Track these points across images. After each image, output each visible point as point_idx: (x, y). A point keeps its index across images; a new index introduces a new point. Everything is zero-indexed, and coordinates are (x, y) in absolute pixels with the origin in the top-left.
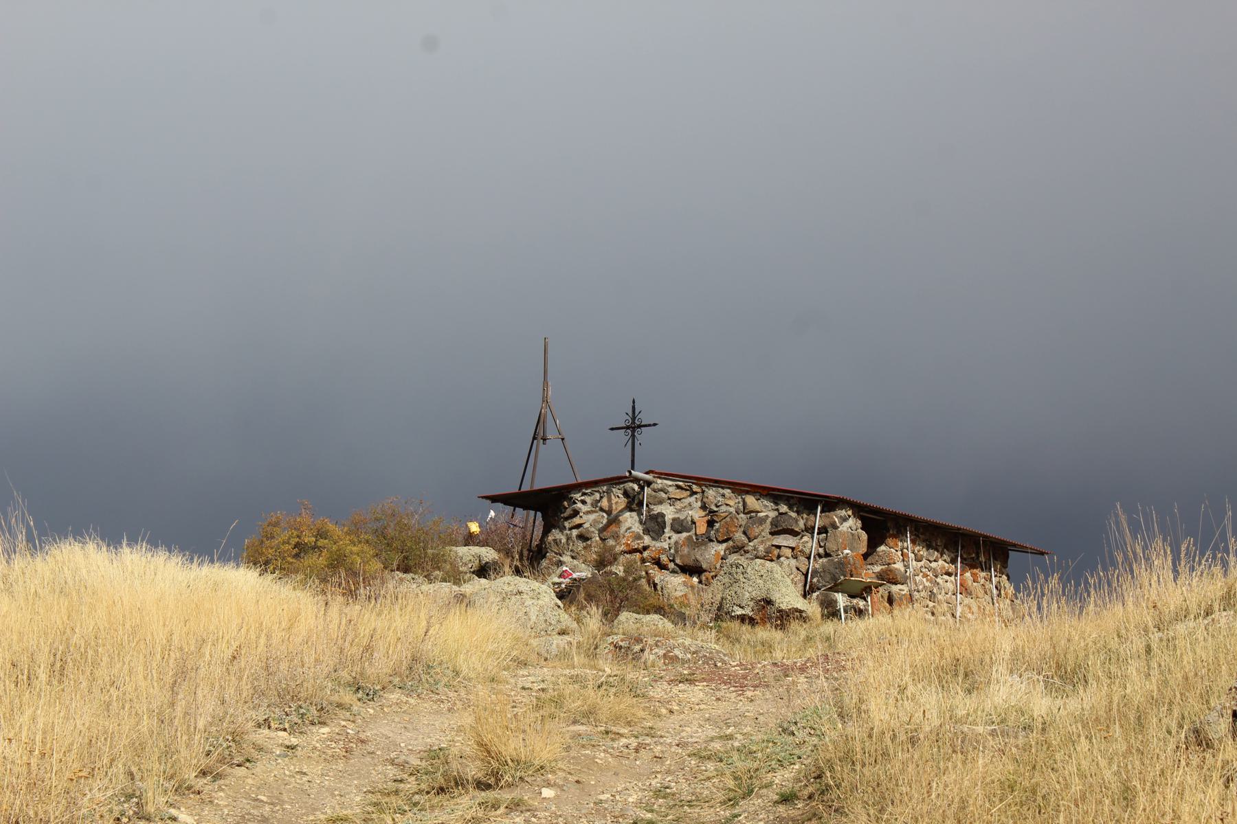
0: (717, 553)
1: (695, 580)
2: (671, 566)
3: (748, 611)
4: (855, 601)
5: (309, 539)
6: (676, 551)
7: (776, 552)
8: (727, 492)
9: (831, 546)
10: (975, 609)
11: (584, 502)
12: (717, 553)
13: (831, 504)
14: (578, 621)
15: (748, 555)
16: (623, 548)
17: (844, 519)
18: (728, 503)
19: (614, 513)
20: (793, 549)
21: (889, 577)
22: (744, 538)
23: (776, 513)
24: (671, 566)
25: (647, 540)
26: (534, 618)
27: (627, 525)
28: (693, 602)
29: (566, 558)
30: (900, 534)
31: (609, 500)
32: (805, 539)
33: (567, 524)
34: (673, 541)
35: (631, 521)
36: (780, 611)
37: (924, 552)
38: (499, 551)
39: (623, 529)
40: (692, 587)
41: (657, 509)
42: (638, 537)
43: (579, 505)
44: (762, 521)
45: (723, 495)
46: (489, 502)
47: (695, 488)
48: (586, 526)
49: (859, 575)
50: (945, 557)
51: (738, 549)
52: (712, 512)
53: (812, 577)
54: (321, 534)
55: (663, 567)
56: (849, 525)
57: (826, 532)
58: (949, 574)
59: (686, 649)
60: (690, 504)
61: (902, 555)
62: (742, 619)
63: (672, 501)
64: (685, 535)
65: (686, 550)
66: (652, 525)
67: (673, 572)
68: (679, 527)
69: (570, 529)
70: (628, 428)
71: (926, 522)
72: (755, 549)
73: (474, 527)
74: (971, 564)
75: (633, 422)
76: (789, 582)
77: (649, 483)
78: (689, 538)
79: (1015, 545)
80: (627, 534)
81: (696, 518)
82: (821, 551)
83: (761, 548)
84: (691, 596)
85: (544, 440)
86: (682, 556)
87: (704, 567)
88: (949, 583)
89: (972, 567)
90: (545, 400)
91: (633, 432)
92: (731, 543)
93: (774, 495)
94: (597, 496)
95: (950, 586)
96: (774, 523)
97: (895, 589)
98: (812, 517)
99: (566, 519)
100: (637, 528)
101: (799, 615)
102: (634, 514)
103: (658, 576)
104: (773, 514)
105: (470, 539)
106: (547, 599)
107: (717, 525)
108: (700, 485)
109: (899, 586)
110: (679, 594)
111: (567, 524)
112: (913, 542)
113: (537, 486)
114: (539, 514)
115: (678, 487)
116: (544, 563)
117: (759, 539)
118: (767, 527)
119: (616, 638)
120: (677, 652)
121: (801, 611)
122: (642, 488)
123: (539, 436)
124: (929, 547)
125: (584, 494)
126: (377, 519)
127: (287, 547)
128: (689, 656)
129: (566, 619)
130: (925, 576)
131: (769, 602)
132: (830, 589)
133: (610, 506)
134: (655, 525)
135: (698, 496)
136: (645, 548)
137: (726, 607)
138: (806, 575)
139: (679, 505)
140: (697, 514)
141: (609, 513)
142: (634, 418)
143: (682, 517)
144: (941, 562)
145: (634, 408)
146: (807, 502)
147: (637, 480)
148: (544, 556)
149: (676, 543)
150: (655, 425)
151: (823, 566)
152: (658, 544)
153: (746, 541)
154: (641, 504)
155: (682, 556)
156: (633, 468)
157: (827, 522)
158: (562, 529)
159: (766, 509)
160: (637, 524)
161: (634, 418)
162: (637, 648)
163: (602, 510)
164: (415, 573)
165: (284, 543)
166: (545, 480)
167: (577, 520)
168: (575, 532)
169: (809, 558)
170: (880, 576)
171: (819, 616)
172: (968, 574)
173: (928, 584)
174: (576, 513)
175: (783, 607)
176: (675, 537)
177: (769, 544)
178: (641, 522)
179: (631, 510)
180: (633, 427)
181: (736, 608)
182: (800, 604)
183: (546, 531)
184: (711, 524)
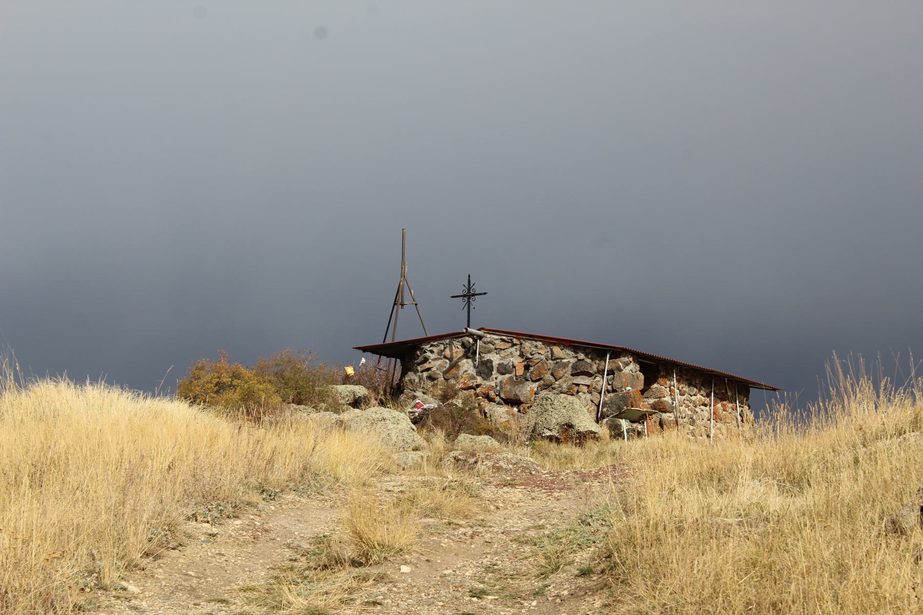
0: (532, 390)
1: (515, 409)
2: (497, 399)
3: (554, 433)
4: (635, 425)
5: (226, 379)
6: (501, 388)
7: (576, 388)
8: (539, 344)
9: (617, 384)
10: (724, 431)
11: (432, 352)
12: (532, 390)
13: (617, 353)
14: (428, 440)
15: (555, 391)
16: (461, 386)
17: (627, 364)
18: (540, 352)
19: (455, 359)
20: (588, 386)
21: (660, 408)
22: (551, 378)
23: (576, 360)
24: (497, 399)
25: (479, 380)
26: (394, 438)
27: (465, 368)
28: (514, 426)
29: (419, 394)
30: (668, 375)
31: (451, 350)
32: (598, 379)
33: (419, 368)
34: (498, 380)
35: (467, 366)
36: (579, 433)
37: (686, 389)
38: (368, 388)
39: (461, 372)
40: (513, 415)
41: (487, 357)
42: (473, 378)
43: (428, 354)
44: (565, 365)
45: (536, 347)
46: (361, 351)
47: (515, 341)
48: (433, 369)
49: (638, 406)
50: (702, 392)
51: (547, 386)
52: (528, 359)
53: (603, 407)
54: (235, 376)
55: (491, 400)
56: (630, 368)
57: (613, 374)
58: (705, 405)
59: (509, 461)
60: (511, 353)
61: (670, 391)
62: (551, 438)
63: (498, 350)
64: (508, 376)
65: (508, 387)
66: (483, 368)
67: (499, 403)
68: (503, 369)
69: (422, 372)
70: (464, 296)
71: (688, 366)
72: (560, 386)
73: (350, 371)
74: (721, 397)
75: (469, 292)
76: (586, 411)
77: (481, 338)
78: (511, 378)
79: (754, 383)
80: (465, 376)
81: (516, 363)
82: (609, 387)
83: (565, 386)
84: (512, 422)
85: (402, 305)
86: (505, 392)
87: (522, 399)
88: (705, 412)
89: (722, 399)
90: (403, 275)
91: (469, 299)
92: (542, 382)
93: (575, 346)
94: (442, 347)
95: (706, 414)
96: (574, 367)
97: (665, 416)
98: (603, 363)
99: (419, 364)
100: (472, 371)
101: (593, 435)
102: (470, 361)
103: (488, 407)
104: (573, 361)
105: (347, 380)
106: (404, 424)
107: (532, 369)
108: (519, 339)
109: (668, 414)
110: (503, 420)
111: (419, 368)
112: (678, 381)
113: (396, 340)
114: (398, 361)
115: (503, 340)
116: (402, 397)
117: (563, 379)
118: (569, 370)
119: (456, 453)
120: (501, 463)
121: (592, 432)
122: (475, 341)
123: (398, 302)
124: (690, 385)
125: (432, 346)
126: (277, 365)
127: (210, 385)
128: (511, 466)
129: (419, 439)
130: (688, 406)
131: (570, 426)
132: (616, 416)
133: (452, 355)
134: (485, 369)
135: (517, 347)
136: (478, 386)
137: (539, 429)
138: (598, 406)
139: (503, 354)
140: (517, 361)
141: (451, 359)
142: (469, 289)
143: (505, 363)
144: (699, 396)
145: (469, 281)
146: (599, 352)
147: (471, 335)
148: (402, 392)
149: (501, 382)
150: (485, 293)
151: (611, 399)
152: (487, 383)
153: (553, 380)
154: (474, 353)
155: (505, 392)
156: (469, 326)
157: (614, 366)
158: (416, 371)
159: (568, 357)
160: (472, 368)
161: (469, 289)
162: (472, 460)
163: (445, 357)
164: (306, 405)
165: (208, 383)
166: (404, 334)
167: (427, 365)
168: (425, 374)
169: (600, 393)
170: (654, 406)
171: (608, 437)
172: (719, 405)
173: (690, 413)
174: (426, 360)
175: (581, 430)
176: (500, 377)
177: (570, 382)
178: (474, 367)
179: (467, 358)
180: (469, 295)
181: (546, 430)
182: (594, 427)
183: (404, 374)
184: (527, 368)
